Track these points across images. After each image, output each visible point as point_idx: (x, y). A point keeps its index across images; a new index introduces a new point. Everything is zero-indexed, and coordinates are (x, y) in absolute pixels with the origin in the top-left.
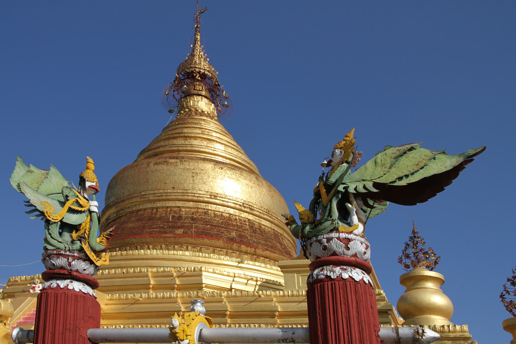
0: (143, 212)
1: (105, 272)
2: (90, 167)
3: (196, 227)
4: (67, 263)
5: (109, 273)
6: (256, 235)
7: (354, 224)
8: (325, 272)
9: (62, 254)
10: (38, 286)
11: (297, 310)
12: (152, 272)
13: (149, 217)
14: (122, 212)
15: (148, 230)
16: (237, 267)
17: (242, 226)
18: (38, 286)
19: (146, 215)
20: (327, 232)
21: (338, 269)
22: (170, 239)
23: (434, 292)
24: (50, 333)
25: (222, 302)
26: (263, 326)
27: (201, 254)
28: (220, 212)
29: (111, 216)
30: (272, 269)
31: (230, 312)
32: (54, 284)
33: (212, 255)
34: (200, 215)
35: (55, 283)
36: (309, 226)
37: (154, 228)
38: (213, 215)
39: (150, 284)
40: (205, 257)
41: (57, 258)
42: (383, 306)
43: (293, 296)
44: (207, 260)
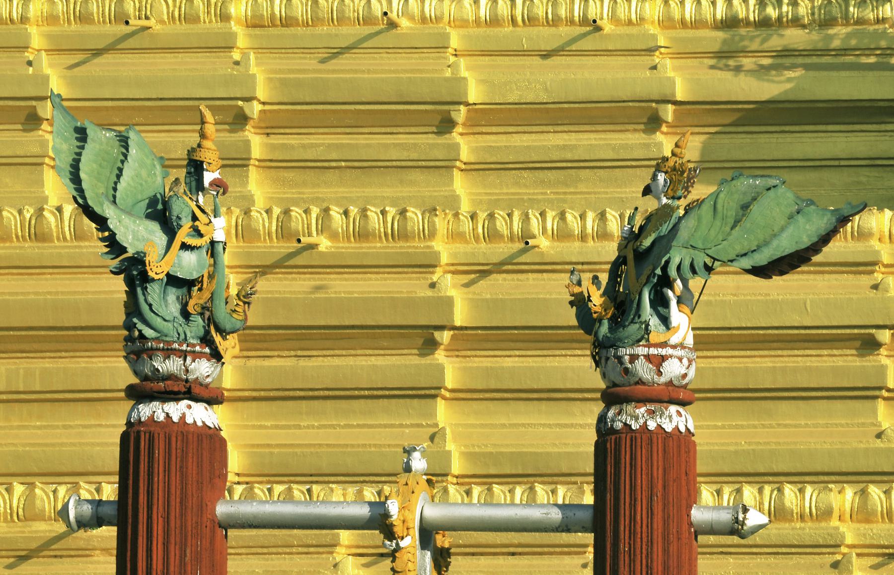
2: (208, 135)
4: (183, 367)
7: (673, 325)
8: (624, 417)
9: (175, 349)
20: (631, 342)
24: (160, 515)
26: (416, 214)
31: (264, 103)
32: (145, 411)
35: (161, 410)
36: (604, 301)
41: (164, 360)
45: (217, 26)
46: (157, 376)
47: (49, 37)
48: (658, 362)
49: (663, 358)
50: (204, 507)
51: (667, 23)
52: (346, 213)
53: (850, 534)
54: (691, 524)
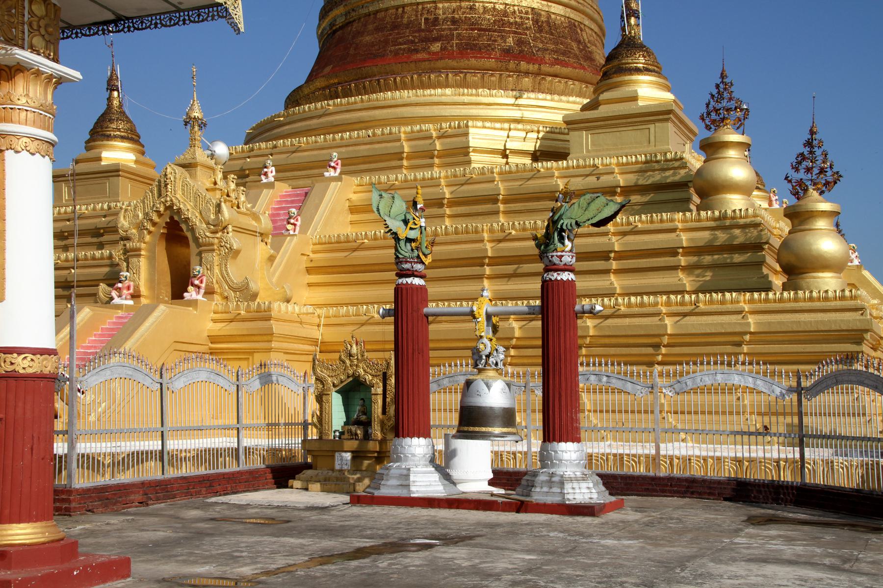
0: (383, 13)
1: (345, 136)
3: (459, 35)
5: (350, 137)
6: (542, 36)
10: (270, 170)
11: (582, 188)
12: (405, 133)
13: (393, 22)
14: (353, 14)
15: (393, 48)
16: (513, 105)
17: (522, 24)
18: (270, 170)
19: (388, 19)
21: (555, 274)
22: (424, 63)
23: (738, 161)
25: (494, 181)
27: (466, 90)
28: (491, 3)
29: (338, 20)
30: (560, 101)
32: (404, 281)
33: (480, 90)
34: (464, 13)
37: (401, 44)
38: (481, 11)
39: (403, 152)
40: (472, 95)
42: (682, 177)
43: (578, 167)
44: (474, 99)
45: (490, 175)
46: (403, 269)
47: (446, 182)
48: (561, 257)
49: (562, 256)
50: (419, 310)
51: (618, 165)
52: (519, 224)
53: (664, 310)
54: (574, 311)
